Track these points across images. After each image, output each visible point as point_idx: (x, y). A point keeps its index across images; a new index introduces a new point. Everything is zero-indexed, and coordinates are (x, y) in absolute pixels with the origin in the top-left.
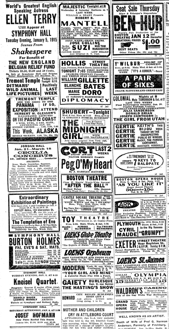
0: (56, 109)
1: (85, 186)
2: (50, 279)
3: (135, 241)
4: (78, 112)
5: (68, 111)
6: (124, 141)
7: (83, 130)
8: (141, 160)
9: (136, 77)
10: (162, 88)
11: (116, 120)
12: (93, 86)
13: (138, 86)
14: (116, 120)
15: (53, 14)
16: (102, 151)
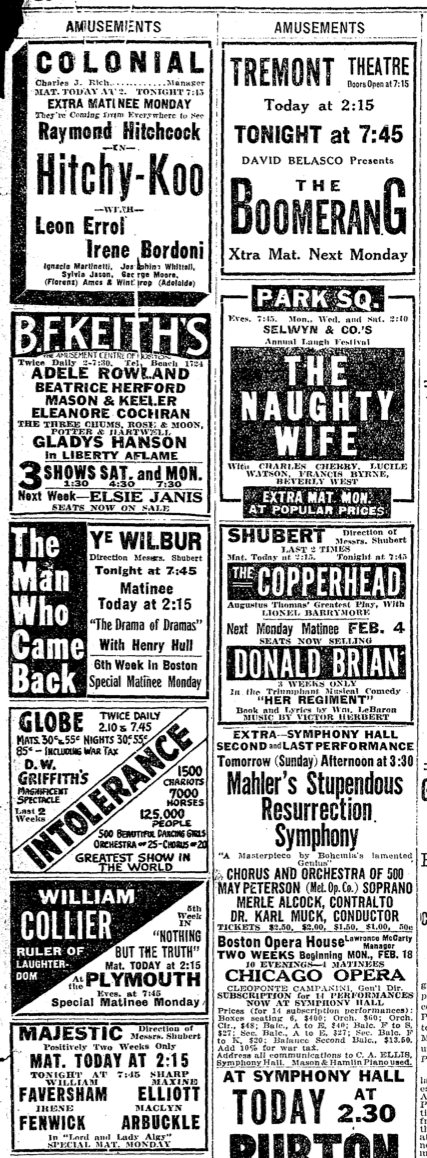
0: (130, 737)
2: (177, 242)
4: (286, 535)
5: (248, 531)
6: (135, 388)
7: (139, 62)
8: (129, 400)
9: (265, 294)
12: (64, 387)
13: (349, 301)
15: (254, 83)
16: (69, 1100)
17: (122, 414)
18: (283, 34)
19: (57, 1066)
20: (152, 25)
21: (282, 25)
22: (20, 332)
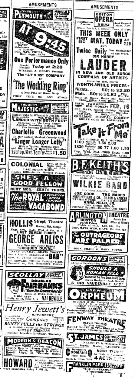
1: (81, 32)
3: (27, 360)
10: (68, 56)
11: (100, 319)
14: (100, 319)
17: (79, 76)
18: (31, 7)
19: (101, 43)
20: (54, 4)
21: (31, 4)
22: (74, 164)
